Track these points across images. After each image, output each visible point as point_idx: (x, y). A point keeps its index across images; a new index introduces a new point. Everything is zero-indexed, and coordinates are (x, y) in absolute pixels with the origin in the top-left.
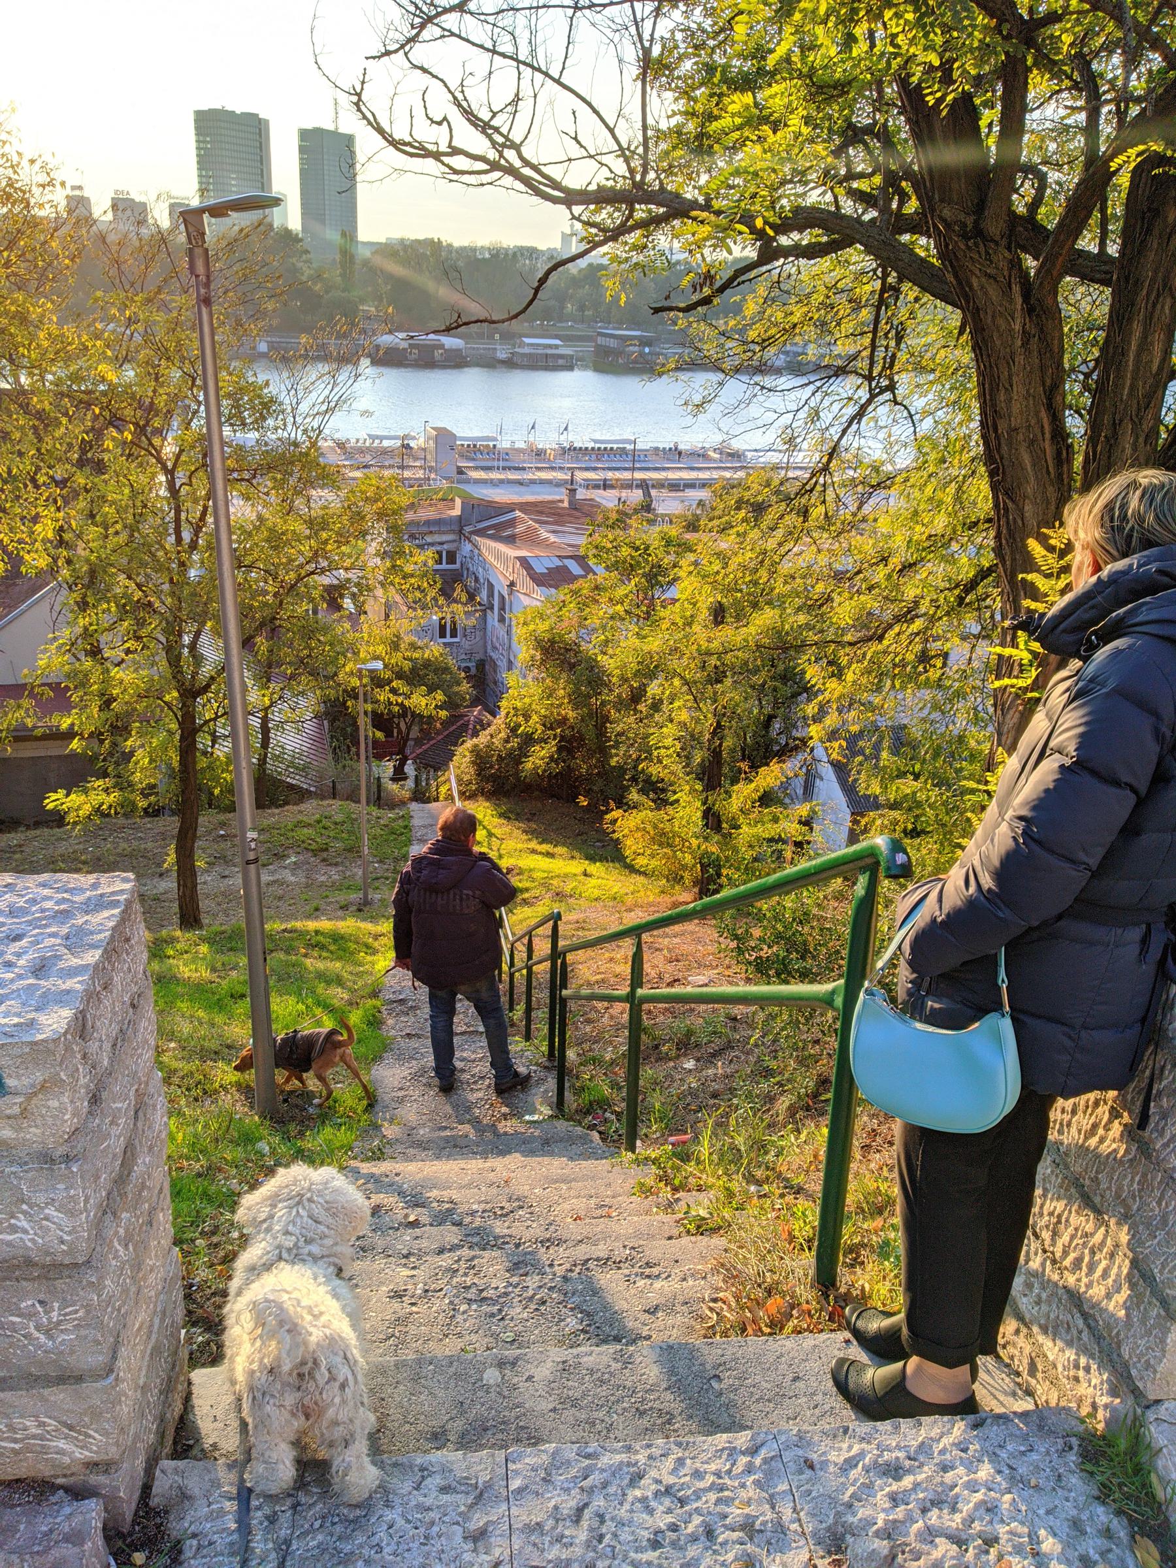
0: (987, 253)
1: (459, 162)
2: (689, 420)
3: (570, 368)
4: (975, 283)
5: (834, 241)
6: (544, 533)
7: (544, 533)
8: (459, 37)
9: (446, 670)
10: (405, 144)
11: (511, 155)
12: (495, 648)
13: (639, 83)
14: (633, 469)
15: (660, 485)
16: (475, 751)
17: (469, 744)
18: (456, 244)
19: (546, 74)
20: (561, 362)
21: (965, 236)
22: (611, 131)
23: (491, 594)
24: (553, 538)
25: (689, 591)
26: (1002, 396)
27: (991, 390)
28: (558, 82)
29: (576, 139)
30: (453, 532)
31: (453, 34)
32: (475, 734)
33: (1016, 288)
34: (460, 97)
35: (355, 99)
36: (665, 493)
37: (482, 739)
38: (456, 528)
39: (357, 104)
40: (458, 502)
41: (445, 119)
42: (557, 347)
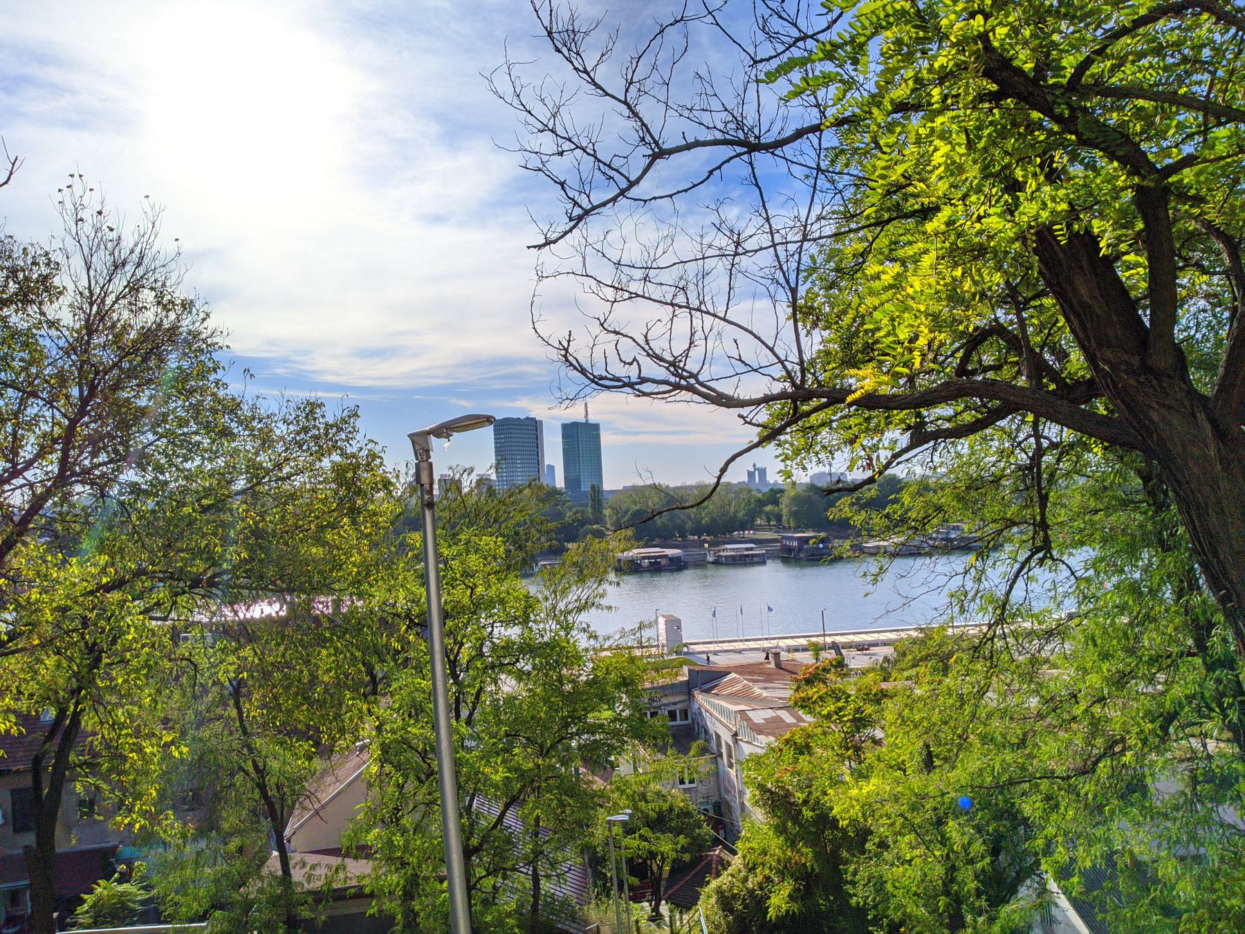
0: (1161, 387)
1: (647, 387)
2: (870, 588)
3: (764, 563)
4: (1154, 416)
5: (978, 421)
6: (757, 690)
7: (757, 690)
8: (643, 297)
9: (688, 814)
10: (602, 378)
11: (692, 381)
12: (728, 791)
13: (792, 321)
14: (824, 635)
15: (849, 646)
16: (719, 891)
17: (714, 884)
18: (672, 486)
19: (714, 315)
20: (755, 559)
21: (1135, 374)
22: (772, 350)
23: (719, 745)
24: (765, 694)
25: (895, 739)
26: (1213, 520)
27: (1199, 517)
28: (724, 319)
29: (740, 360)
30: (683, 693)
31: (638, 296)
32: (718, 875)
33: (1201, 417)
34: (647, 348)
35: (563, 352)
36: (854, 652)
37: (724, 880)
38: (685, 689)
39: (565, 356)
40: (685, 669)
41: (635, 359)
42: (752, 549)
